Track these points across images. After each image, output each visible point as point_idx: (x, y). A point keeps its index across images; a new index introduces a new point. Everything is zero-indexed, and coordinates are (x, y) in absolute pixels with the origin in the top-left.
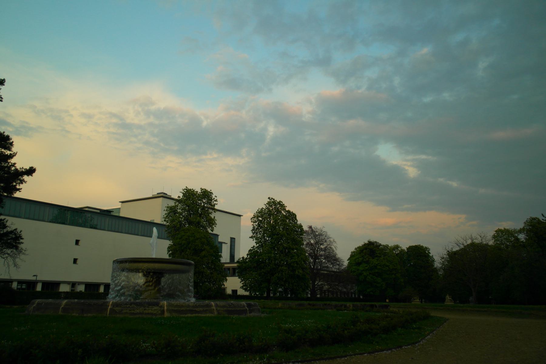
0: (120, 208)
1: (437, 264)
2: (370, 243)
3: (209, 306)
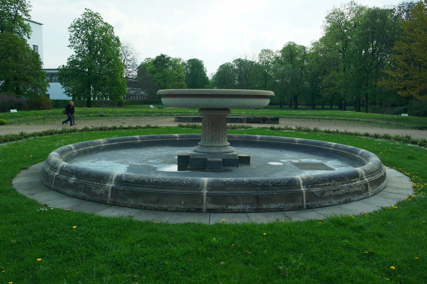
2: (163, 56)
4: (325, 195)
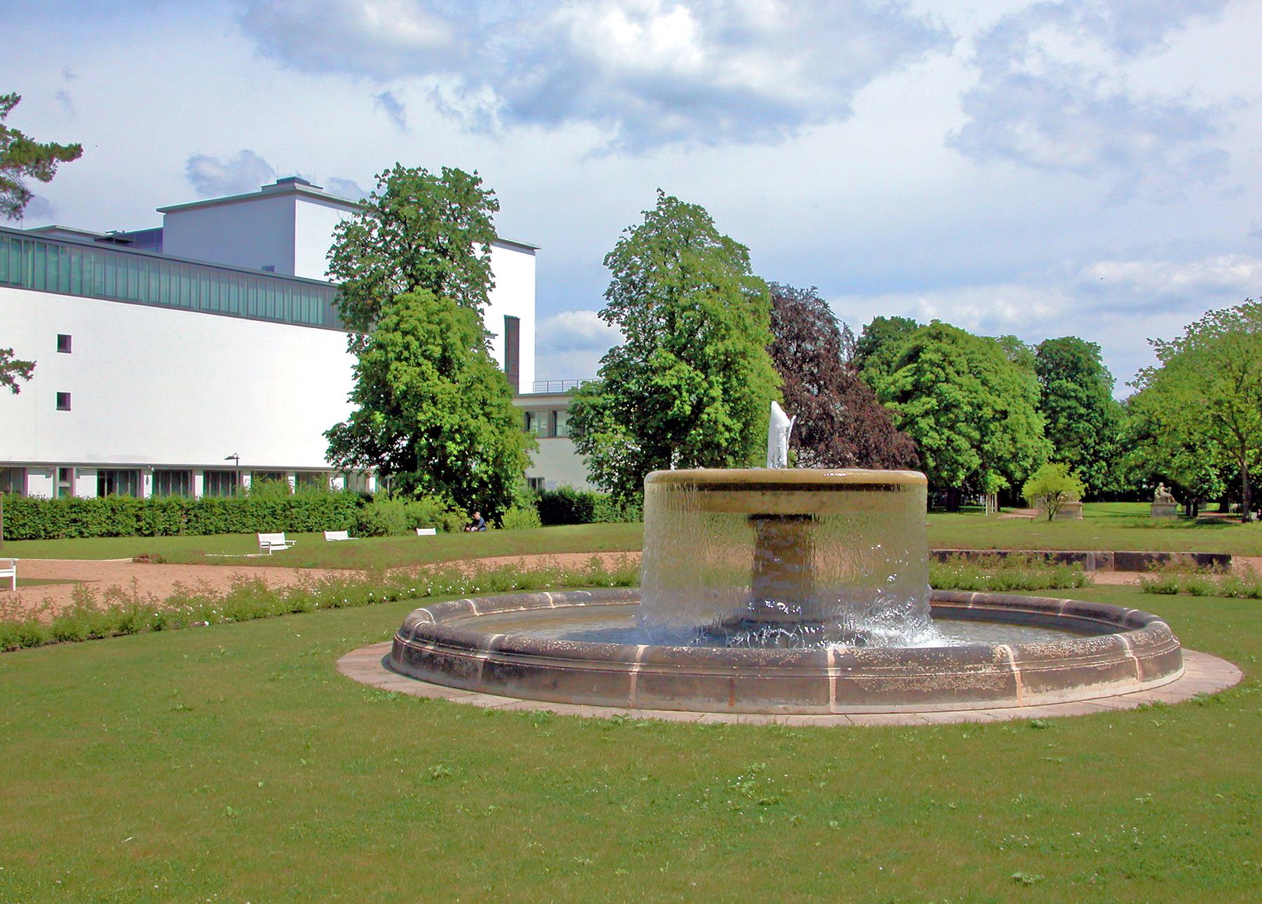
1: (1120, 394)
4: (882, 690)
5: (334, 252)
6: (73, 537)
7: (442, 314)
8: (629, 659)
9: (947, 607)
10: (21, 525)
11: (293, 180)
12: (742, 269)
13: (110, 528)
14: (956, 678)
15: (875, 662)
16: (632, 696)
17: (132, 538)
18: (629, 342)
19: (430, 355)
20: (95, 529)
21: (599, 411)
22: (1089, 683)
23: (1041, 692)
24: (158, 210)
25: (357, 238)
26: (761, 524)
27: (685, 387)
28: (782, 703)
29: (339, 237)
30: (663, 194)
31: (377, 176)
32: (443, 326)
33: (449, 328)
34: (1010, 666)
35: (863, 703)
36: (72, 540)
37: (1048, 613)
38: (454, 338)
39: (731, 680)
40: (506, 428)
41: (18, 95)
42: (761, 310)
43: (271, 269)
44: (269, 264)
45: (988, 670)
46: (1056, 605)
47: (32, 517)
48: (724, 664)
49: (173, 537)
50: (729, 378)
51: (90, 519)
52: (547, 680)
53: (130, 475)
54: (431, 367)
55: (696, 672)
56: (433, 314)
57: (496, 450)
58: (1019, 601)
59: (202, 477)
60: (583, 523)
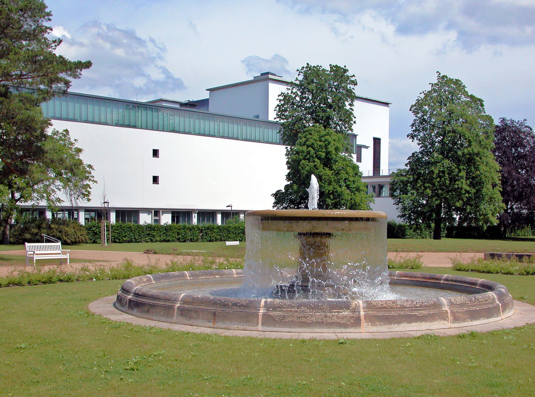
0: (208, 100)
3: (437, 305)
4: (285, 320)
5: (278, 108)
6: (148, 242)
7: (326, 137)
8: (175, 300)
9: (432, 282)
10: (124, 236)
11: (268, 73)
12: (480, 111)
13: (165, 238)
14: (326, 316)
15: (284, 306)
16: (175, 318)
17: (175, 243)
18: (421, 149)
19: (320, 156)
20: (158, 239)
21: (405, 184)
22: (410, 322)
23: (377, 325)
24: (206, 90)
25: (289, 101)
26: (303, 238)
27: (447, 172)
28: (236, 325)
29: (280, 101)
30: (440, 74)
31: (298, 70)
32: (326, 143)
33: (329, 143)
34: (360, 311)
35: (275, 326)
36: (147, 243)
37: (473, 286)
38: (331, 149)
39: (215, 312)
40: (356, 192)
41: (61, 39)
42: (489, 132)
43: (258, 117)
44: (257, 114)
45: (346, 313)
46: (477, 282)
47: (129, 233)
48: (213, 304)
49: (195, 243)
50: (470, 166)
51: (155, 234)
52: (146, 308)
53: (187, 214)
54: (319, 163)
55: (200, 307)
56: (322, 137)
57: (351, 203)
58: (464, 280)
59: (221, 215)
60: (400, 238)
